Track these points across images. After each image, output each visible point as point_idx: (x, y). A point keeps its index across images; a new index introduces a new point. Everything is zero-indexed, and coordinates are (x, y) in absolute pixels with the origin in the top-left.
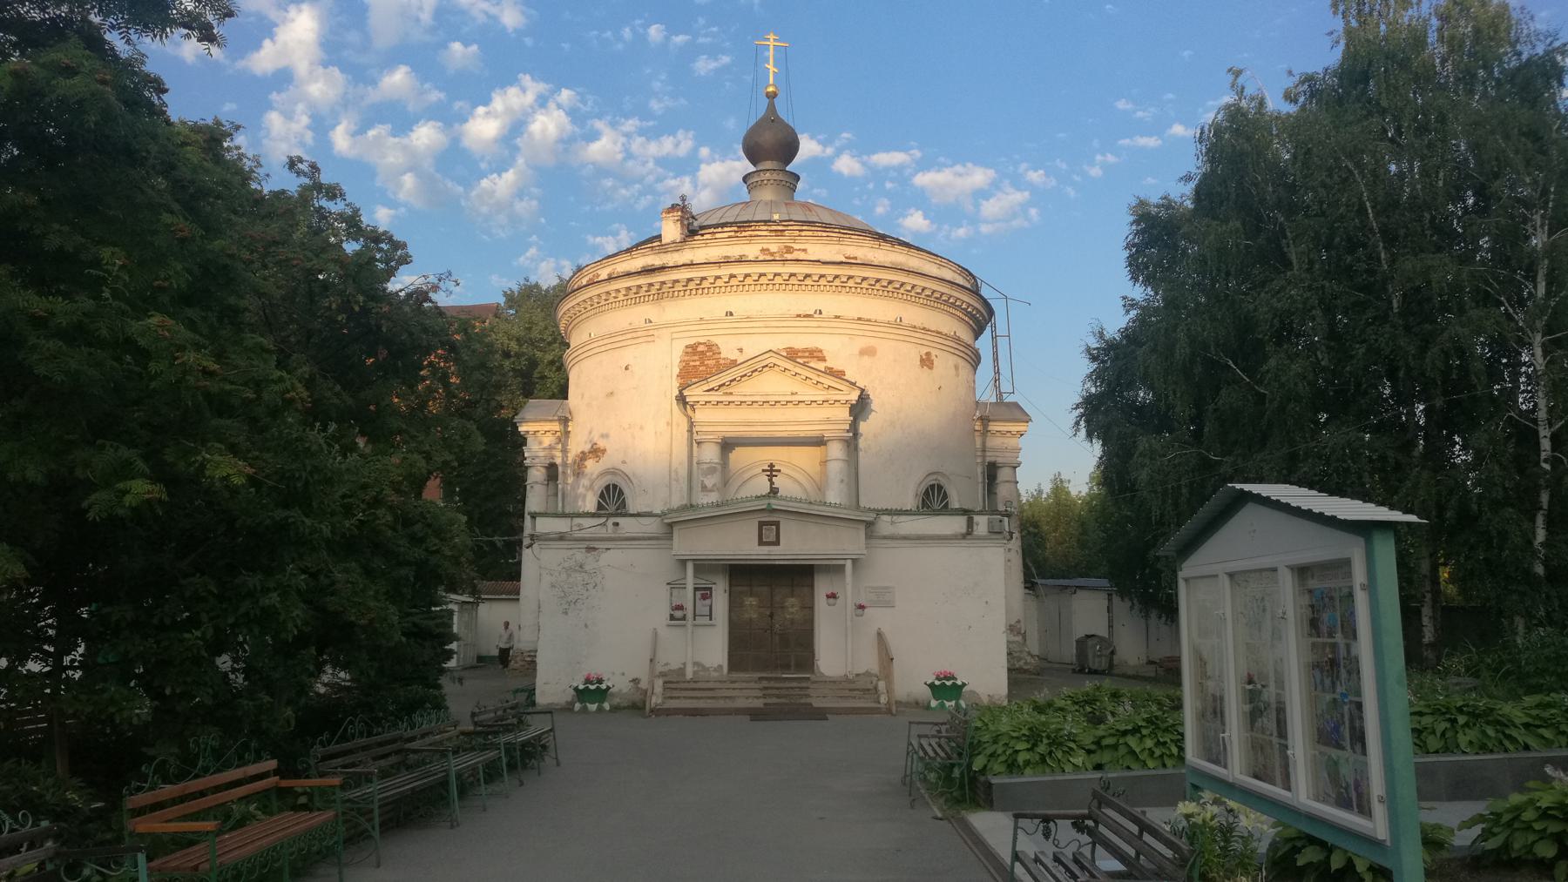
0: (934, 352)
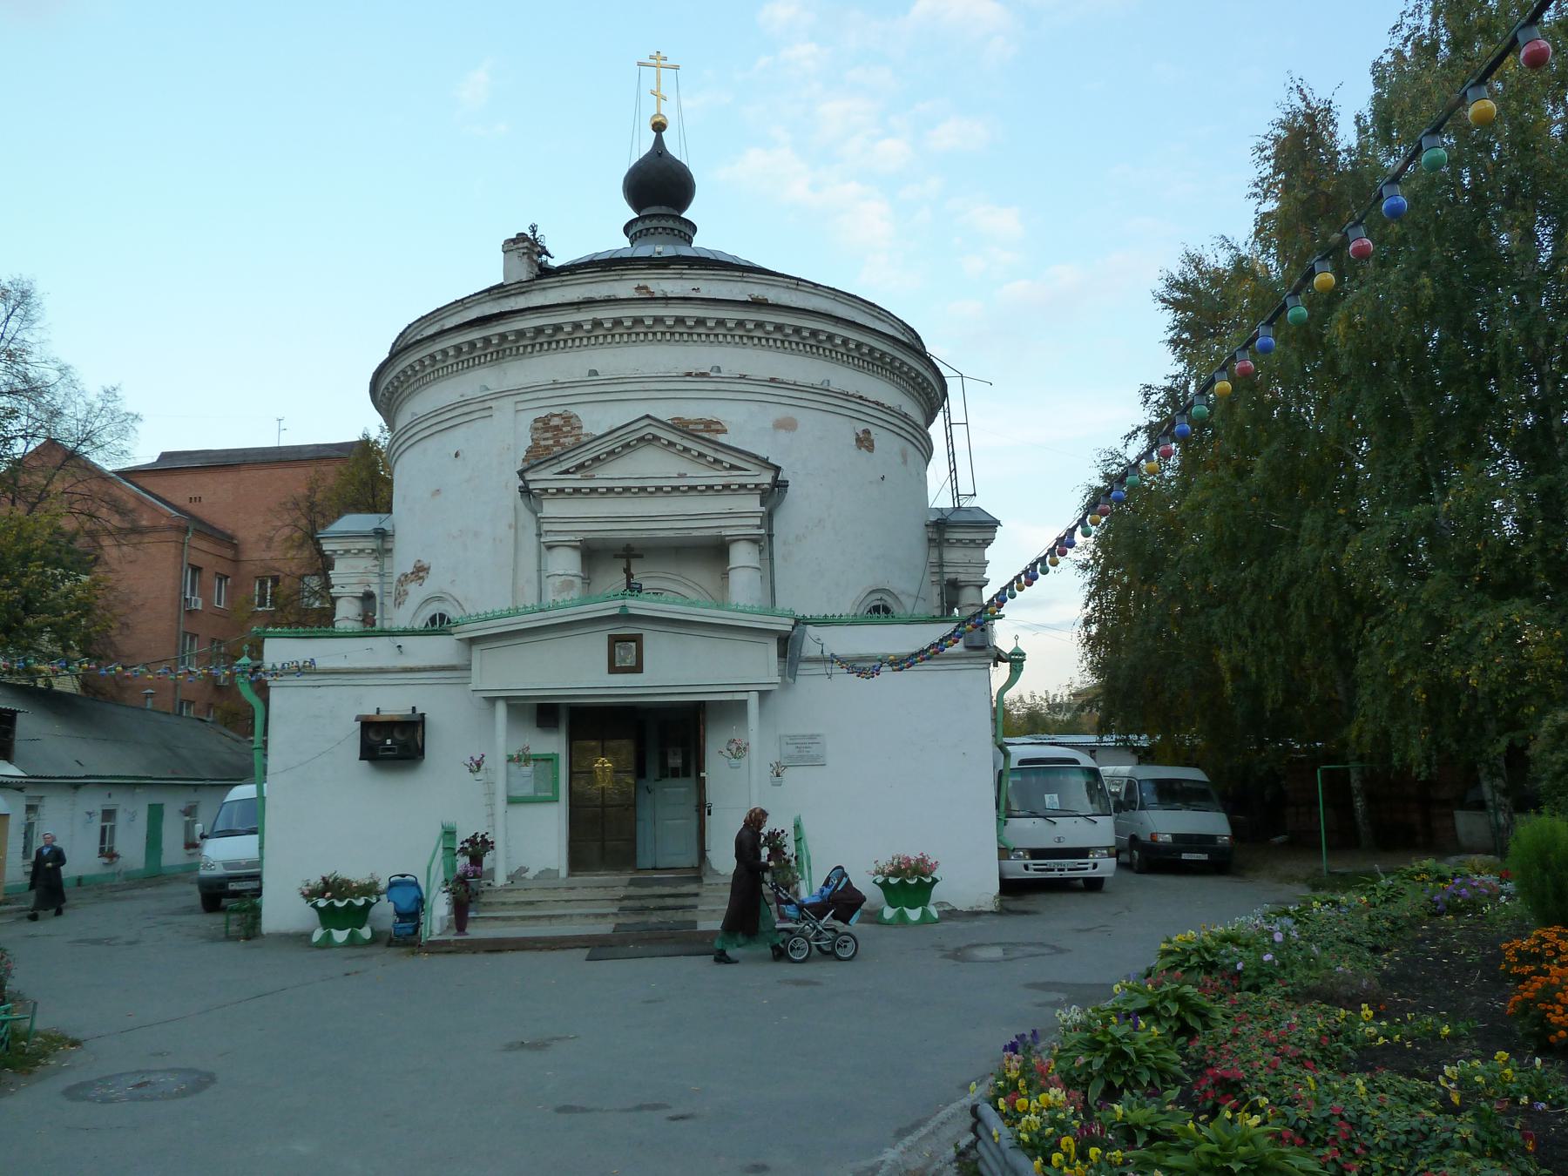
0: (874, 430)
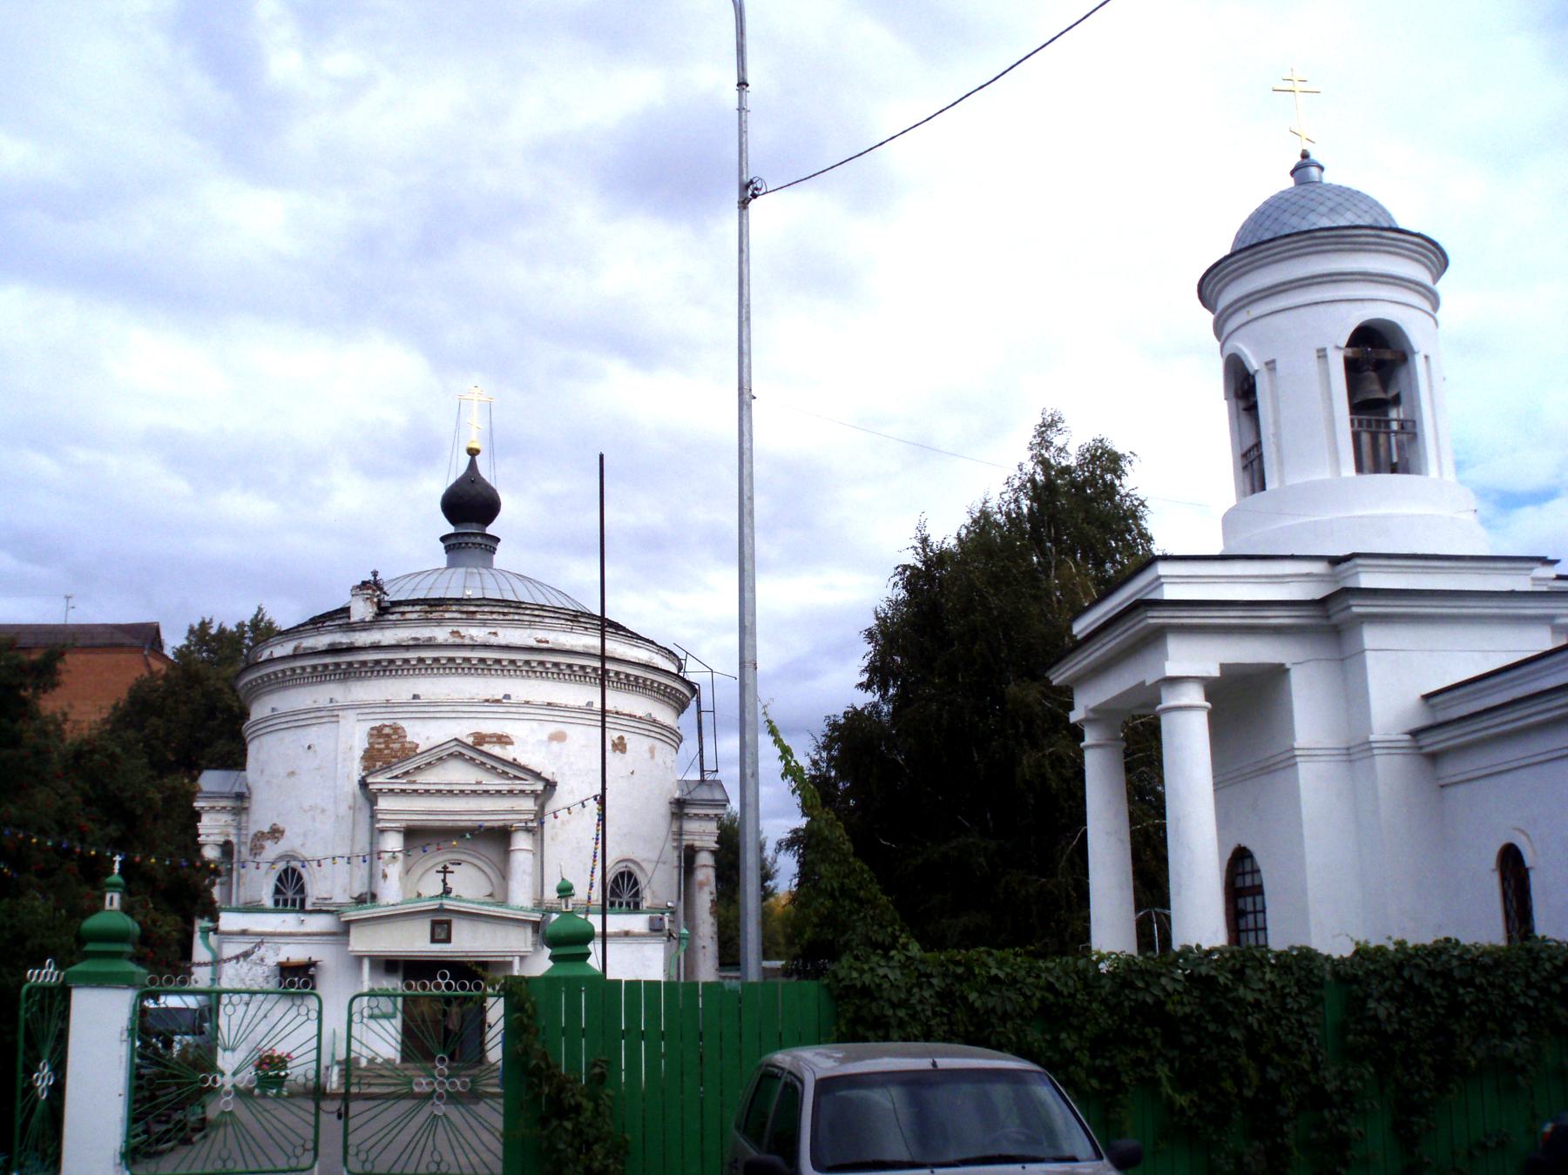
0: (626, 736)
